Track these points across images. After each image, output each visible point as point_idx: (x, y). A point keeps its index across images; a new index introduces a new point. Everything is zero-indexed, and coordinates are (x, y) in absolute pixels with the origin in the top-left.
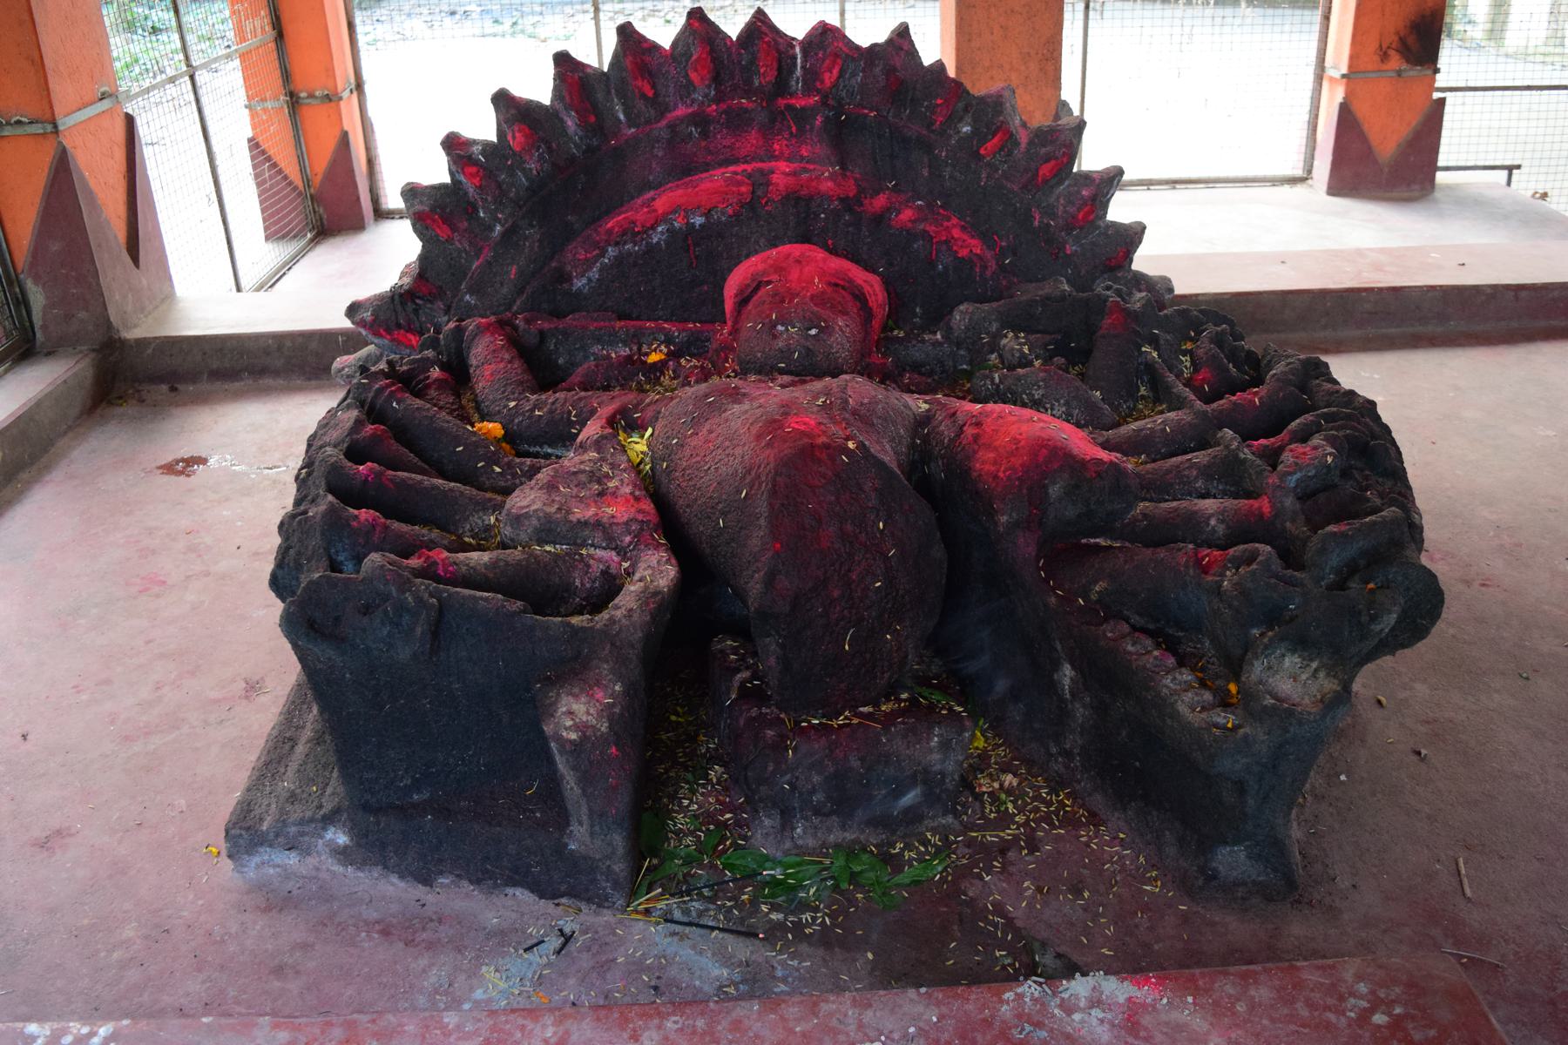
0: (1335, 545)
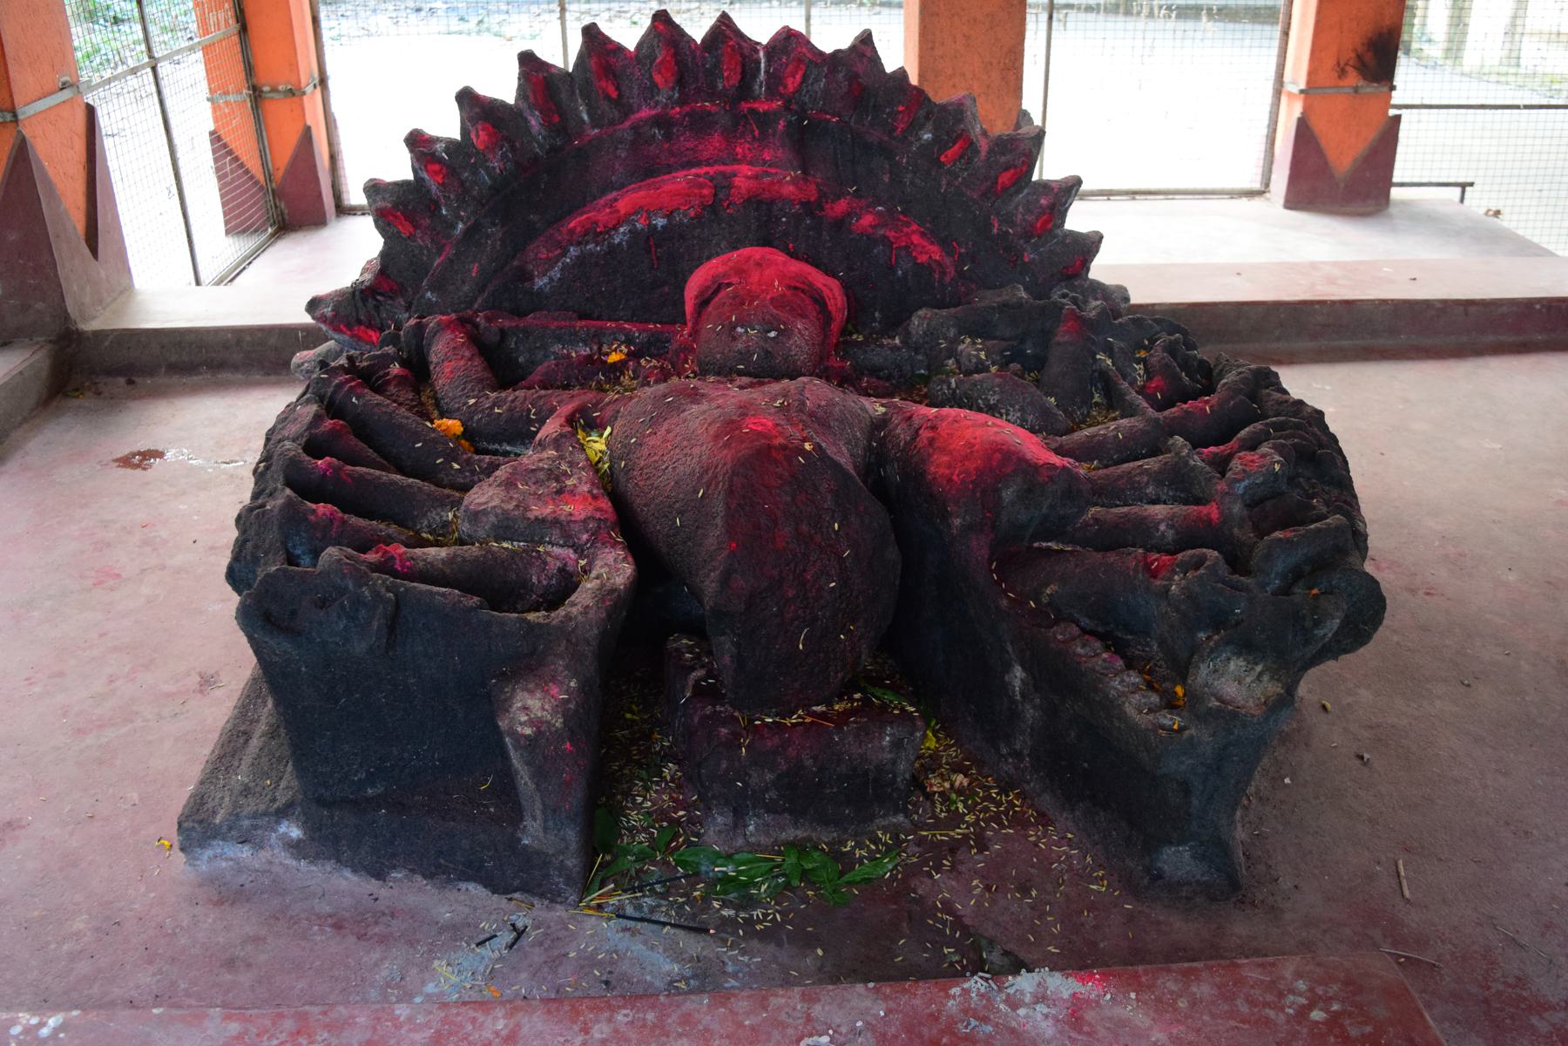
0: (1282, 549)
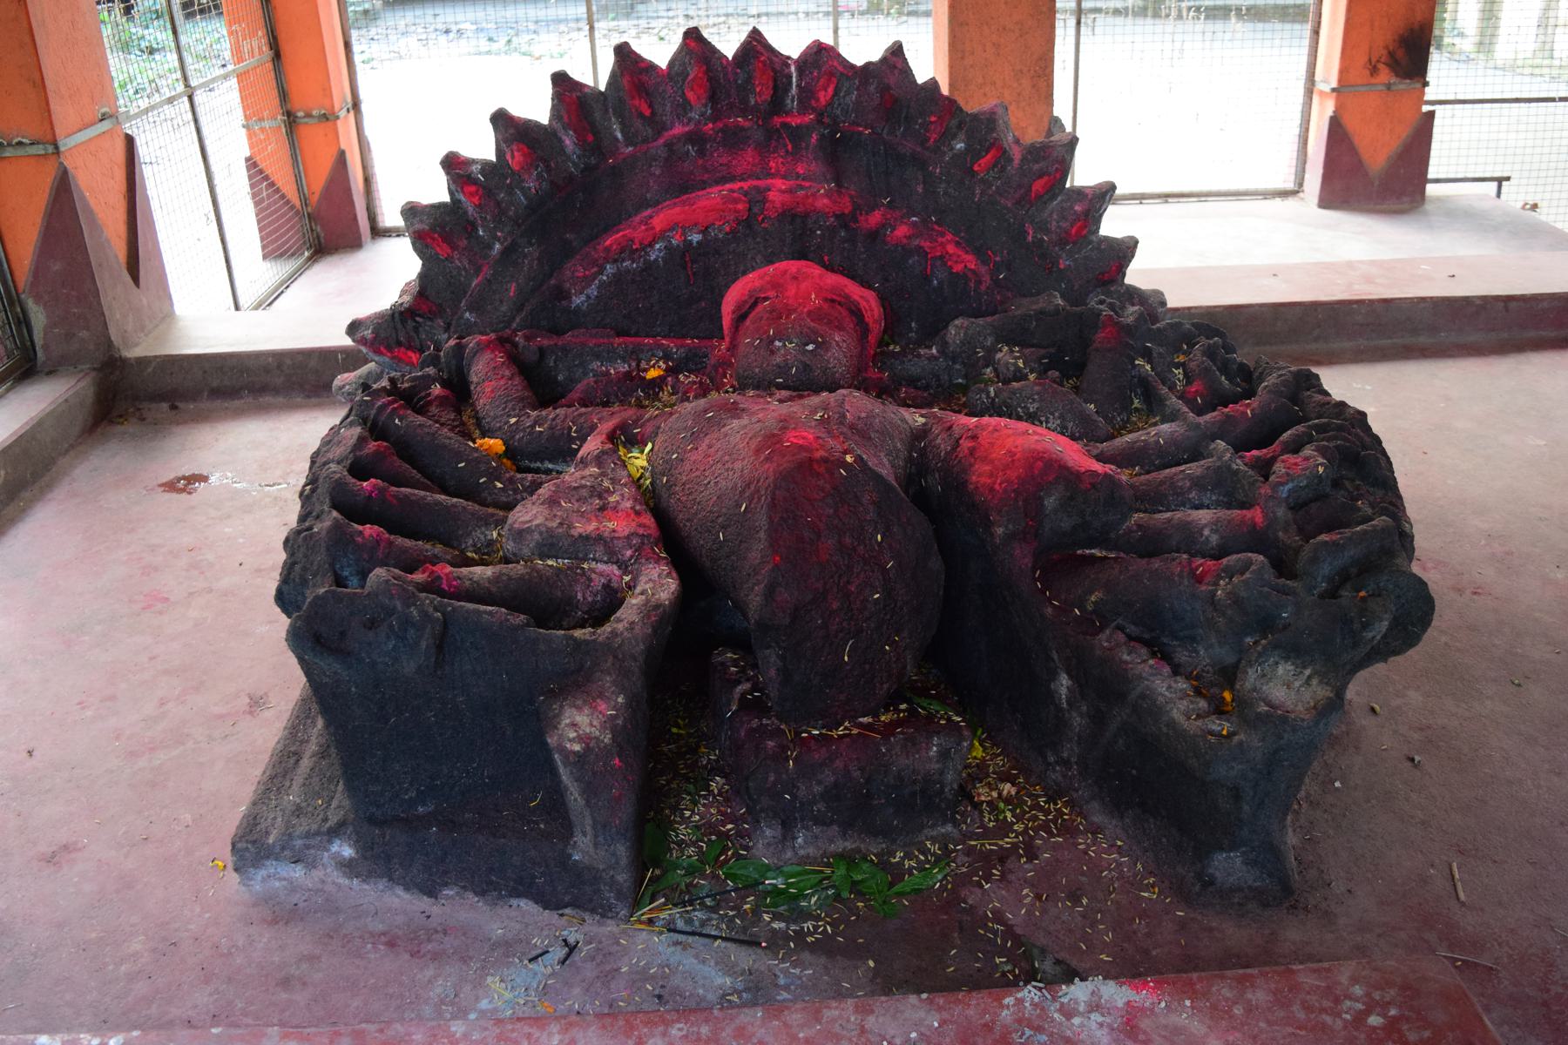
0: (1326, 554)
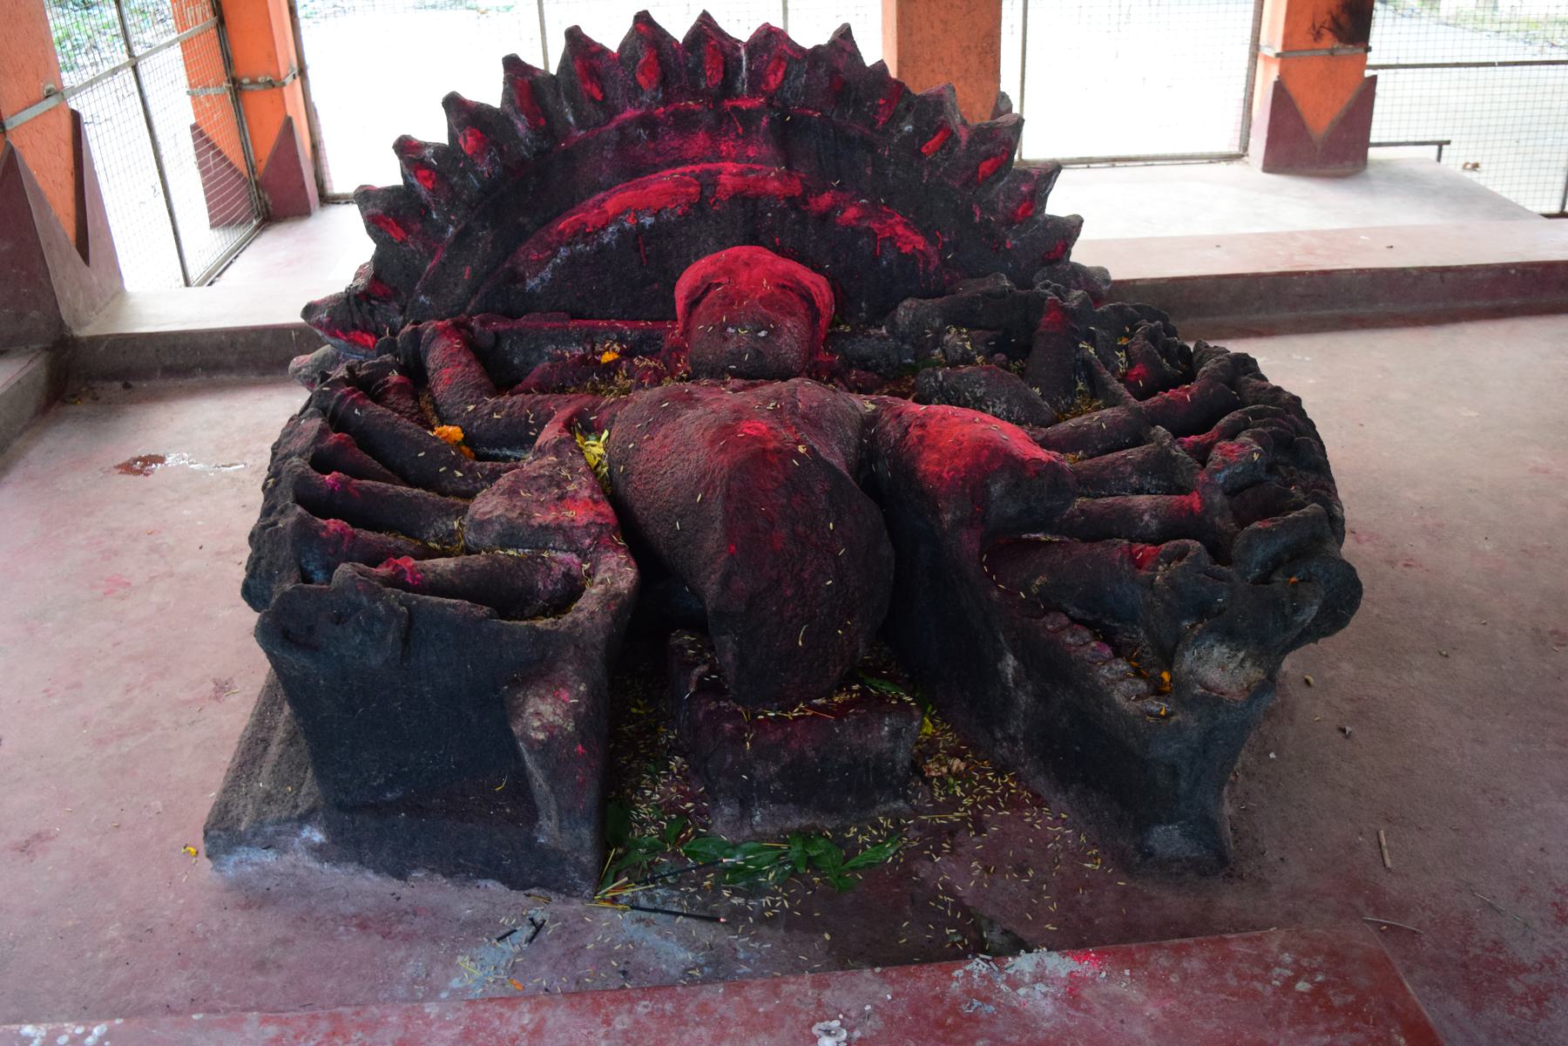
0: (1260, 540)
